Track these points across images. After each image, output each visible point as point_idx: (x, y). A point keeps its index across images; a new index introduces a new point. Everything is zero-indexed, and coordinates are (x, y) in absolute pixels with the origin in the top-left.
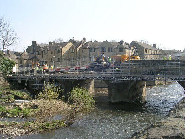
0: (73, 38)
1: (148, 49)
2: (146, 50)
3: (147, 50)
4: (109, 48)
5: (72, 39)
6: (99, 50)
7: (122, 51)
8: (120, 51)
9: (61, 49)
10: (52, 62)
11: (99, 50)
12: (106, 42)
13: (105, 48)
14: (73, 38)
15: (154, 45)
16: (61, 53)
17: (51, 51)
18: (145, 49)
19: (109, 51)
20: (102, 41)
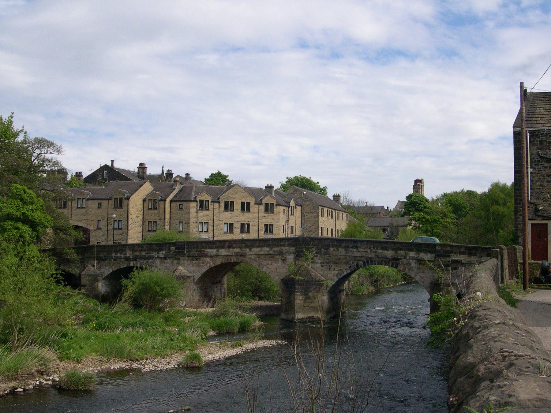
0: (112, 161)
1: (326, 207)
2: (323, 210)
3: (325, 209)
4: (243, 204)
5: (110, 165)
6: (219, 206)
7: (272, 212)
8: (266, 210)
9: (128, 199)
10: (99, 228)
11: (219, 206)
12: (296, 178)
13: (232, 203)
14: (112, 161)
15: (142, 167)
16: (125, 209)
17: (100, 201)
18: (320, 208)
19: (243, 209)
20: (482, 188)
